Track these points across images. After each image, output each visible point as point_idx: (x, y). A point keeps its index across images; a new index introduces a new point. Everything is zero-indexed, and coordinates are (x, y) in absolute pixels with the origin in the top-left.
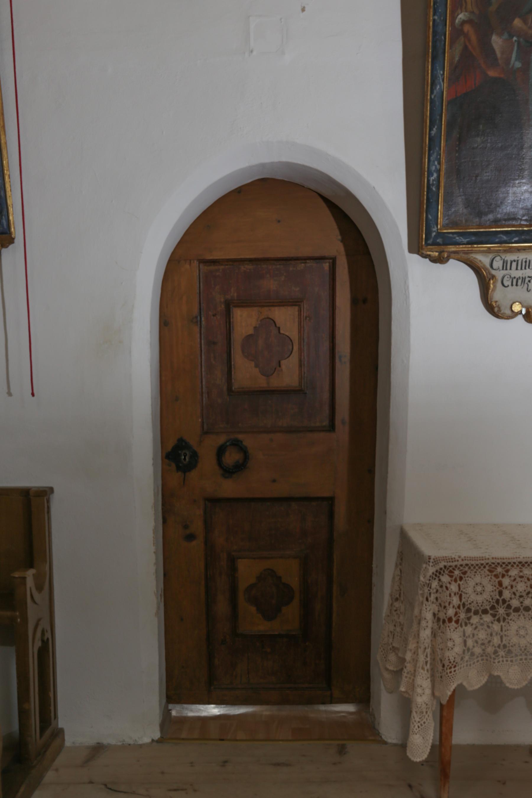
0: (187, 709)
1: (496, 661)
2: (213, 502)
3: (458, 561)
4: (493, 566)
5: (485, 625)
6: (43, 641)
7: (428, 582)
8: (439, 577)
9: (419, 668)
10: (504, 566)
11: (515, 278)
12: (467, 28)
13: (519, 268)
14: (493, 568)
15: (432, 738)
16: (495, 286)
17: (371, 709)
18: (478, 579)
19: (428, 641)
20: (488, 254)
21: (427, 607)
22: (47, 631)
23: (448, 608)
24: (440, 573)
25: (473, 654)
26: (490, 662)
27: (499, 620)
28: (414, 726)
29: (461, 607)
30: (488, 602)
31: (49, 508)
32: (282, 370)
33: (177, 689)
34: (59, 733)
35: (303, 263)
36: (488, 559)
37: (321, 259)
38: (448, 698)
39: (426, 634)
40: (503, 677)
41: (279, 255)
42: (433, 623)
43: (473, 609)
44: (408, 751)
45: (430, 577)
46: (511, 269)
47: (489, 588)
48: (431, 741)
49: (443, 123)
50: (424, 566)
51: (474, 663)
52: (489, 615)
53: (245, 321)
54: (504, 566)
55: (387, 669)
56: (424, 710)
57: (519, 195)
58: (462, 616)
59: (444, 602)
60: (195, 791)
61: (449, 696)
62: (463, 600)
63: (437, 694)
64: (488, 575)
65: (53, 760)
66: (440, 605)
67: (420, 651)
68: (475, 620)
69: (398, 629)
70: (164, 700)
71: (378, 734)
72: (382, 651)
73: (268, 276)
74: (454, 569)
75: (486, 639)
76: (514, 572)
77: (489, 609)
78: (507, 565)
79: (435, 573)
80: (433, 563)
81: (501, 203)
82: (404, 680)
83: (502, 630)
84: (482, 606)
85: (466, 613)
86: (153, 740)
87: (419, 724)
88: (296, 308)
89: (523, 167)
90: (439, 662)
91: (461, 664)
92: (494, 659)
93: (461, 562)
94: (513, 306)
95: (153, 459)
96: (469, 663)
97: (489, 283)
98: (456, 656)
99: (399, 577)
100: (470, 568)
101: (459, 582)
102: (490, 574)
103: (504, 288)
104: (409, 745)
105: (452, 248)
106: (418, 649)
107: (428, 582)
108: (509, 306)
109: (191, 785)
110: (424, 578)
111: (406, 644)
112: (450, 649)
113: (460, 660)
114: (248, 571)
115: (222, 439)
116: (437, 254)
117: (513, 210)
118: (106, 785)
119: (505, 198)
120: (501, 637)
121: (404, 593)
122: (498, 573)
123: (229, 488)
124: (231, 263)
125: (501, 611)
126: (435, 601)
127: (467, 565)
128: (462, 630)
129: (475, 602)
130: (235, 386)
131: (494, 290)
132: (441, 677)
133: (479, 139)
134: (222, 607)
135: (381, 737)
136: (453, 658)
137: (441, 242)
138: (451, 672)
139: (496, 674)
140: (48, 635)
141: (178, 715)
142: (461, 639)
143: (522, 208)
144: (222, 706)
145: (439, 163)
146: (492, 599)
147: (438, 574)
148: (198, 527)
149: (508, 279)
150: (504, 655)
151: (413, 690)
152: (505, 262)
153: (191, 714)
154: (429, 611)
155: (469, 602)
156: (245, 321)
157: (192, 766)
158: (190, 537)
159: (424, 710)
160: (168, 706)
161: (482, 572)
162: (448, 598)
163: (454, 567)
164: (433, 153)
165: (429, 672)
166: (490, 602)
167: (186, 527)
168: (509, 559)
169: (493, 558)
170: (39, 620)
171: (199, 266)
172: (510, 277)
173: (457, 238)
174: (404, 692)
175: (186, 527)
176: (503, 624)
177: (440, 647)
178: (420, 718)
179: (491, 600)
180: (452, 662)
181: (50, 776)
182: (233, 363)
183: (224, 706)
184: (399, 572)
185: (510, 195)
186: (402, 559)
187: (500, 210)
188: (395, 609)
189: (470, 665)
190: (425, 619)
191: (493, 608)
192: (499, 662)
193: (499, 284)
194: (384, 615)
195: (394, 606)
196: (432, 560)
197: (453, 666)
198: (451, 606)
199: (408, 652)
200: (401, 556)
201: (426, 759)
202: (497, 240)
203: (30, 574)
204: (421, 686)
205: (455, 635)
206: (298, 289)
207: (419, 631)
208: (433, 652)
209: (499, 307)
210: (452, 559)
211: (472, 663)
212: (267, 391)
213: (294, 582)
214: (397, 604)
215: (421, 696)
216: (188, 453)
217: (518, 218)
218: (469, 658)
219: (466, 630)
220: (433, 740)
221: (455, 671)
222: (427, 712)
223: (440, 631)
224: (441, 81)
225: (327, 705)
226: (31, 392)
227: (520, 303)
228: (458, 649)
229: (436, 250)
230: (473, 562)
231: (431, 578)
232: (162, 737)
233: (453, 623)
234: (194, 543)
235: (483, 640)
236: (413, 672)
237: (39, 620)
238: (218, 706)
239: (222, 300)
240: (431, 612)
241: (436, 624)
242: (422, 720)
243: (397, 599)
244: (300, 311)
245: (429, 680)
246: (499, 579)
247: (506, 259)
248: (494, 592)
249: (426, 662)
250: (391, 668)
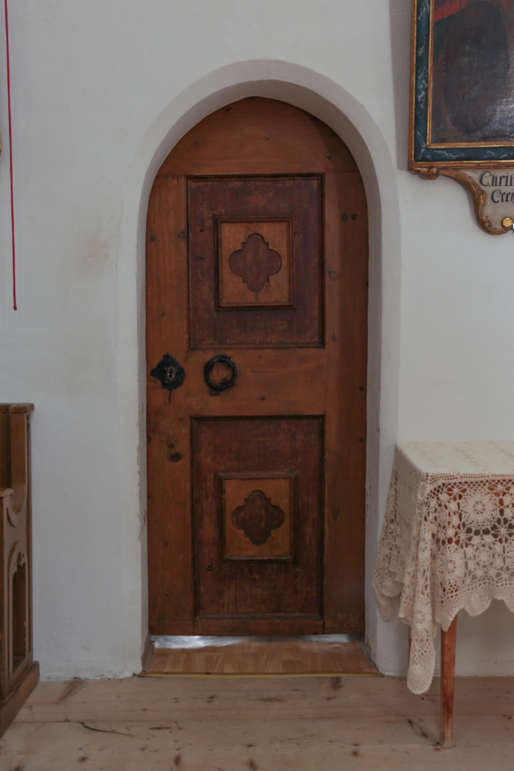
0: (170, 640)
1: (499, 584)
2: (200, 420)
3: (457, 478)
4: (493, 483)
5: (487, 546)
6: (19, 566)
7: (426, 500)
8: (437, 495)
9: (418, 592)
10: (504, 483)
11: (505, 193)
13: (509, 184)
14: (493, 486)
15: (433, 668)
16: (485, 202)
17: (366, 639)
18: (478, 497)
19: (428, 563)
20: (477, 170)
21: (425, 527)
22: (23, 556)
23: (447, 528)
24: (438, 491)
25: (474, 577)
26: (493, 585)
27: (501, 541)
28: (415, 655)
29: (462, 527)
30: (488, 522)
31: (28, 425)
32: (271, 286)
33: (160, 619)
34: (34, 667)
35: (292, 180)
36: (488, 476)
37: (310, 176)
38: (449, 625)
39: (425, 556)
40: (507, 602)
41: (268, 172)
42: (432, 544)
43: (474, 529)
44: (408, 683)
45: (428, 495)
46: (500, 185)
47: (490, 506)
48: (432, 672)
49: (430, 43)
50: (422, 483)
51: (476, 587)
52: (490, 536)
53: (232, 236)
54: (504, 483)
55: (383, 596)
56: (425, 638)
57: (507, 113)
58: (463, 536)
59: (443, 522)
60: (180, 729)
61: (450, 622)
62: (463, 520)
63: (438, 620)
64: (489, 493)
65: (27, 696)
66: (439, 525)
67: (420, 574)
68: (476, 540)
69: (395, 552)
70: (147, 631)
71: (375, 666)
72: (377, 577)
73: (256, 192)
74: (453, 487)
75: (488, 560)
77: (490, 529)
78: (507, 483)
79: (433, 491)
80: (431, 480)
81: (489, 120)
82: (403, 606)
83: (504, 552)
84: (482, 525)
85: (467, 533)
86: (134, 675)
87: (420, 653)
88: (285, 224)
89: (510, 86)
90: (440, 586)
91: (463, 588)
92: (497, 582)
93: (459, 480)
94: (504, 222)
95: (138, 375)
96: (470, 587)
97: (479, 199)
98: (458, 579)
99: (394, 497)
100: (469, 486)
101: (458, 500)
102: (490, 492)
103: (494, 203)
104: (410, 677)
105: (442, 164)
106: (417, 572)
107: (426, 500)
108: (499, 222)
109: (176, 723)
110: (422, 496)
111: (404, 568)
112: (451, 572)
113: (461, 583)
114: (236, 492)
115: (209, 356)
116: (426, 170)
117: (500, 127)
118: (83, 723)
119: (493, 116)
120: (504, 559)
121: (399, 514)
122: (499, 490)
123: (217, 406)
124: (219, 179)
125: (503, 531)
126: (434, 520)
127: (466, 482)
128: (463, 551)
129: (475, 522)
130: (224, 302)
131: (484, 205)
132: (442, 602)
133: (466, 60)
134: (208, 531)
135: (377, 669)
136: (454, 582)
137: (431, 159)
138: (452, 597)
139: (499, 598)
140: (25, 560)
141: (161, 647)
142: (462, 561)
143: (510, 126)
144: (208, 637)
145: (427, 82)
146: (493, 518)
147: (436, 492)
148: (183, 446)
149: (498, 195)
150: (507, 578)
151: (413, 616)
152: (494, 178)
153: (174, 646)
154: (428, 531)
155: (469, 521)
156: (232, 236)
157: (176, 702)
158: (176, 457)
159: (425, 638)
160: (150, 638)
161: (482, 490)
162: (448, 517)
163: (453, 485)
164: (421, 72)
165: (430, 597)
166: (491, 521)
167: (171, 446)
168: (509, 476)
169: (493, 475)
170: (16, 544)
171: (187, 182)
172: (500, 192)
173: (446, 154)
174: (402, 619)
175: (171, 446)
176: (506, 545)
177: (440, 569)
178: (421, 647)
179: (492, 519)
180: (453, 586)
181: (23, 714)
182: (220, 278)
183: (211, 637)
184: (394, 492)
185: (498, 113)
186: (396, 479)
187: (488, 128)
188: (390, 531)
189: (472, 589)
190: (424, 540)
191: (494, 528)
192: (502, 585)
193: (489, 200)
194: (379, 538)
195: (390, 528)
196: (429, 478)
197: (454, 590)
198: (451, 525)
199: (406, 575)
200: (396, 476)
201: (428, 691)
202: (486, 157)
203: (8, 492)
204: (421, 612)
205: (455, 556)
206: (286, 205)
207: (417, 553)
208: (433, 575)
209: (489, 222)
210: (450, 476)
211: (474, 586)
212: (256, 307)
213: (284, 504)
214: (392, 526)
215: (421, 622)
216: (174, 370)
217: (507, 135)
218: (471, 582)
219: (466, 552)
220: (435, 673)
221: (456, 595)
222: (427, 640)
223: (439, 553)
224: (427, 3)
225: (319, 636)
226: (13, 305)
227: (511, 218)
228: (459, 572)
229: (425, 166)
230: (472, 480)
231: (429, 497)
232: (144, 671)
233: (453, 544)
234: (179, 463)
235: (484, 562)
236: (412, 597)
237: (16, 544)
238: (204, 637)
239: (210, 215)
240: (430, 532)
241: (435, 545)
242: (423, 649)
243: (392, 521)
244: (288, 227)
245: (429, 605)
246: (499, 498)
247: (495, 175)
248: (495, 511)
249: (426, 586)
250: (387, 594)
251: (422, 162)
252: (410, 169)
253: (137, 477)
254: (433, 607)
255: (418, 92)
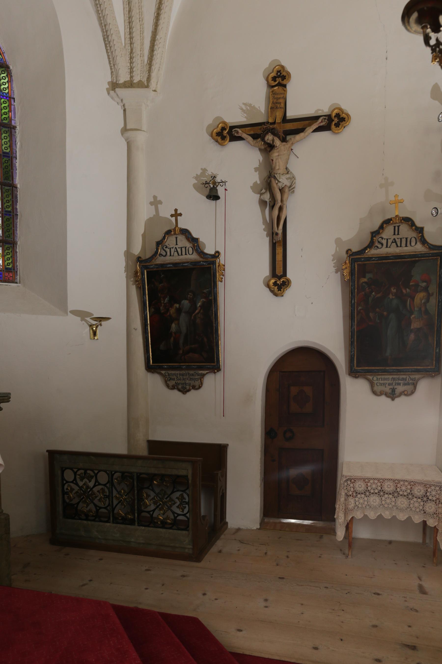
12: (362, 311)
18: (360, 483)
25: (358, 507)
34: (226, 523)
39: (342, 499)
40: (368, 515)
47: (363, 486)
53: (294, 390)
58: (354, 494)
68: (359, 496)
70: (262, 515)
76: (372, 481)
105: (360, 374)
125: (368, 494)
152: (377, 378)
156: (294, 390)
181: (222, 536)
191: (365, 492)
193: (376, 385)
205: (351, 500)
251: (353, 373)
252: (349, 375)
253: (259, 468)
254: (345, 515)
255: (351, 352)
